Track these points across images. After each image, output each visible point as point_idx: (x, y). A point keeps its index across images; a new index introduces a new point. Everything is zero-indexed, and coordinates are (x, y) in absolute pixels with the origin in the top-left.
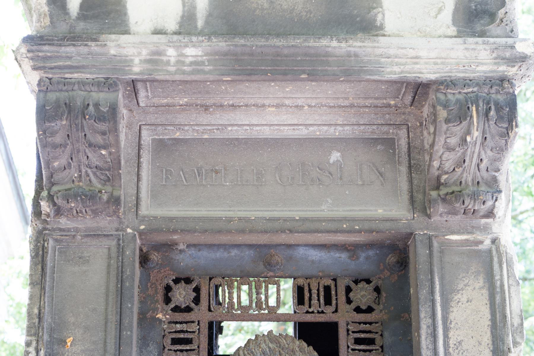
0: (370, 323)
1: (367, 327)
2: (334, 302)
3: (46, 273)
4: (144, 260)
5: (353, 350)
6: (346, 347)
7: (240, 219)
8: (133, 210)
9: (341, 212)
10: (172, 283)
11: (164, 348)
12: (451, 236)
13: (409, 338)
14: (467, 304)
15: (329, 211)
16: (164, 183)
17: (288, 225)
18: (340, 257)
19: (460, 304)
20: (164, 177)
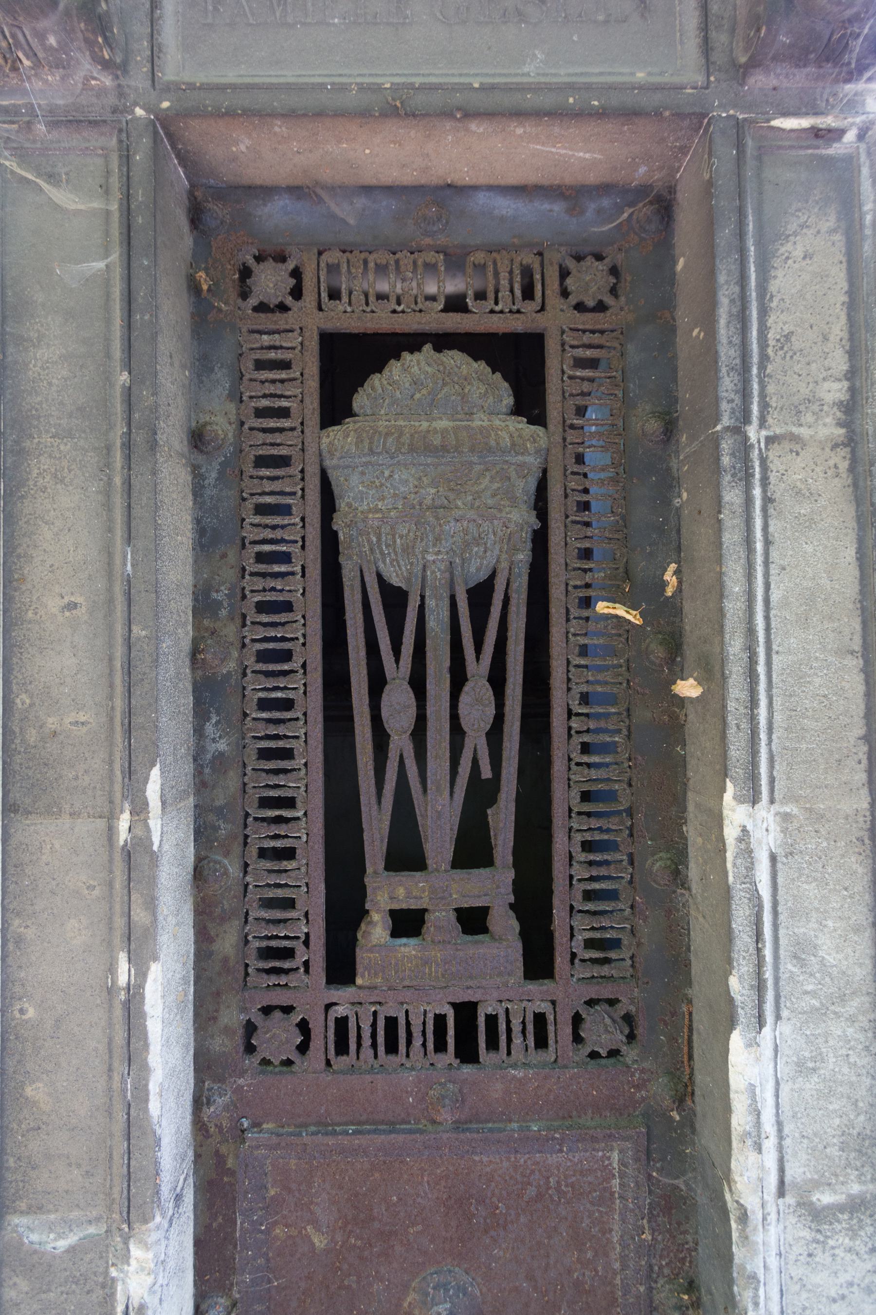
0: (602, 332)
1: (596, 339)
2: (331, 1025)
3: (206, 540)
4: (196, 216)
5: (571, 378)
6: (559, 372)
7: (362, 88)
8: (145, 69)
9: (563, 74)
10: (251, 262)
11: (242, 375)
12: (782, 120)
13: (670, 355)
14: (804, 263)
15: (538, 74)
16: (209, 21)
17: (458, 98)
18: (551, 211)
19: (790, 262)
20: (210, 8)
